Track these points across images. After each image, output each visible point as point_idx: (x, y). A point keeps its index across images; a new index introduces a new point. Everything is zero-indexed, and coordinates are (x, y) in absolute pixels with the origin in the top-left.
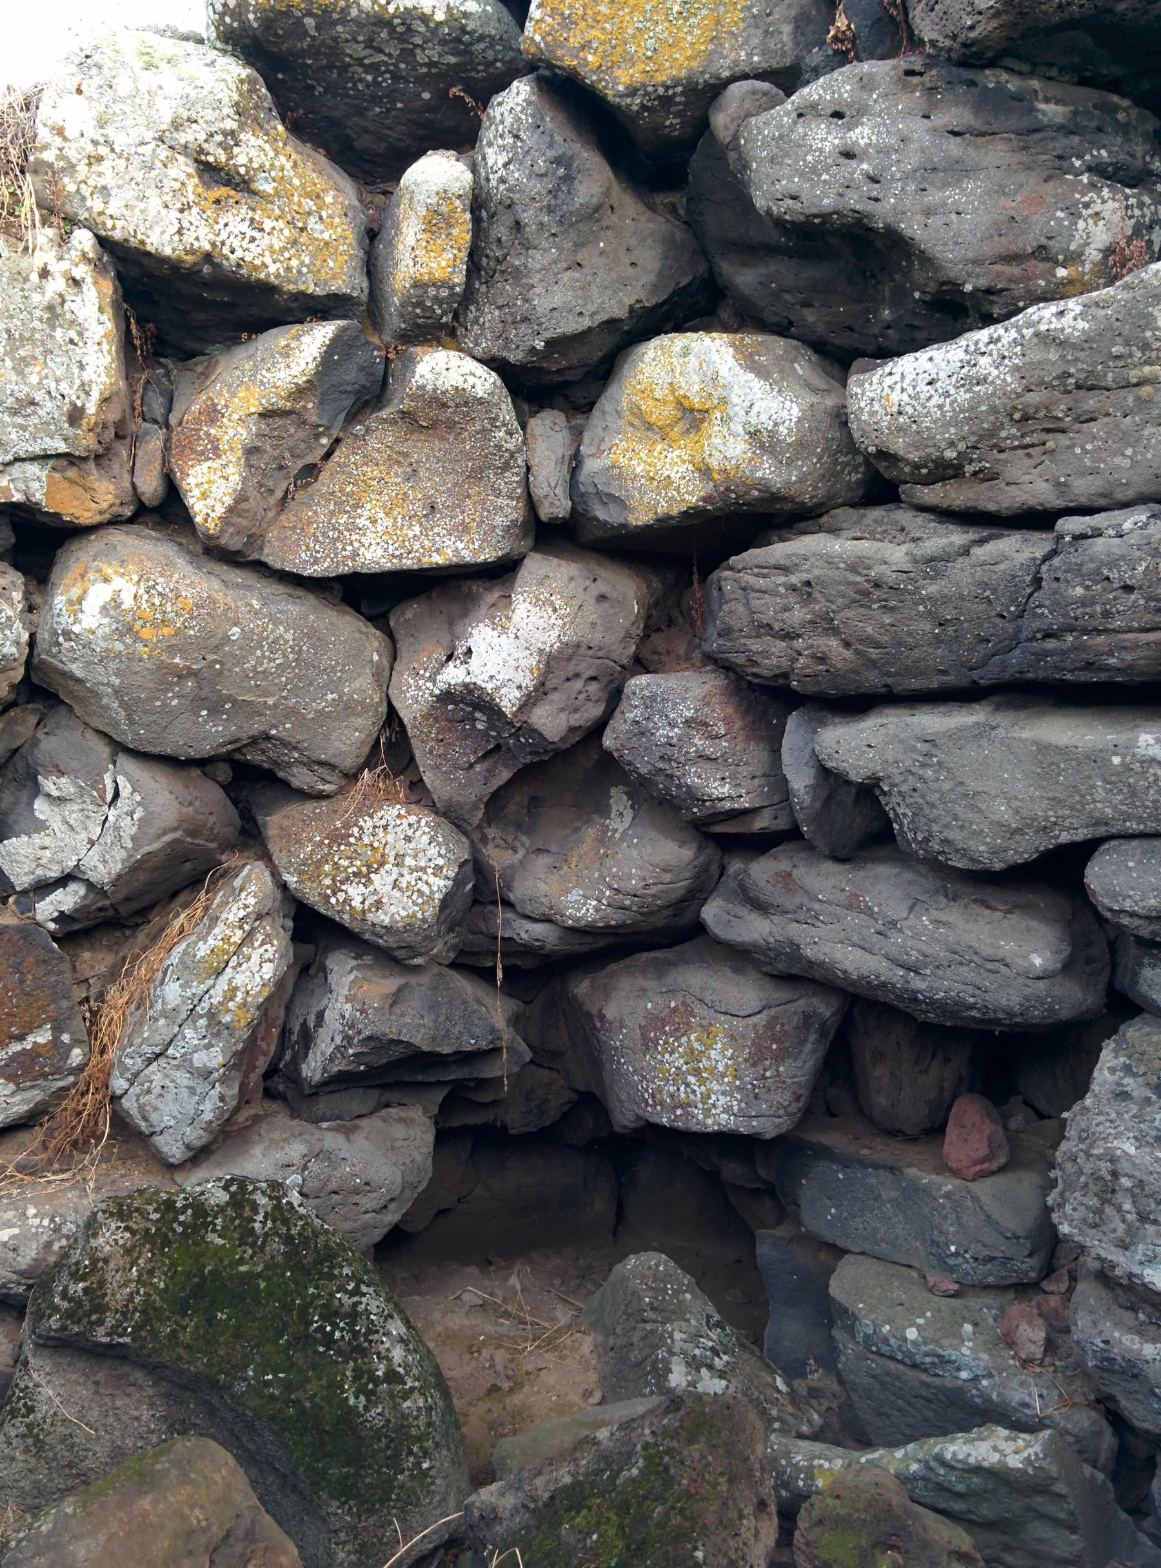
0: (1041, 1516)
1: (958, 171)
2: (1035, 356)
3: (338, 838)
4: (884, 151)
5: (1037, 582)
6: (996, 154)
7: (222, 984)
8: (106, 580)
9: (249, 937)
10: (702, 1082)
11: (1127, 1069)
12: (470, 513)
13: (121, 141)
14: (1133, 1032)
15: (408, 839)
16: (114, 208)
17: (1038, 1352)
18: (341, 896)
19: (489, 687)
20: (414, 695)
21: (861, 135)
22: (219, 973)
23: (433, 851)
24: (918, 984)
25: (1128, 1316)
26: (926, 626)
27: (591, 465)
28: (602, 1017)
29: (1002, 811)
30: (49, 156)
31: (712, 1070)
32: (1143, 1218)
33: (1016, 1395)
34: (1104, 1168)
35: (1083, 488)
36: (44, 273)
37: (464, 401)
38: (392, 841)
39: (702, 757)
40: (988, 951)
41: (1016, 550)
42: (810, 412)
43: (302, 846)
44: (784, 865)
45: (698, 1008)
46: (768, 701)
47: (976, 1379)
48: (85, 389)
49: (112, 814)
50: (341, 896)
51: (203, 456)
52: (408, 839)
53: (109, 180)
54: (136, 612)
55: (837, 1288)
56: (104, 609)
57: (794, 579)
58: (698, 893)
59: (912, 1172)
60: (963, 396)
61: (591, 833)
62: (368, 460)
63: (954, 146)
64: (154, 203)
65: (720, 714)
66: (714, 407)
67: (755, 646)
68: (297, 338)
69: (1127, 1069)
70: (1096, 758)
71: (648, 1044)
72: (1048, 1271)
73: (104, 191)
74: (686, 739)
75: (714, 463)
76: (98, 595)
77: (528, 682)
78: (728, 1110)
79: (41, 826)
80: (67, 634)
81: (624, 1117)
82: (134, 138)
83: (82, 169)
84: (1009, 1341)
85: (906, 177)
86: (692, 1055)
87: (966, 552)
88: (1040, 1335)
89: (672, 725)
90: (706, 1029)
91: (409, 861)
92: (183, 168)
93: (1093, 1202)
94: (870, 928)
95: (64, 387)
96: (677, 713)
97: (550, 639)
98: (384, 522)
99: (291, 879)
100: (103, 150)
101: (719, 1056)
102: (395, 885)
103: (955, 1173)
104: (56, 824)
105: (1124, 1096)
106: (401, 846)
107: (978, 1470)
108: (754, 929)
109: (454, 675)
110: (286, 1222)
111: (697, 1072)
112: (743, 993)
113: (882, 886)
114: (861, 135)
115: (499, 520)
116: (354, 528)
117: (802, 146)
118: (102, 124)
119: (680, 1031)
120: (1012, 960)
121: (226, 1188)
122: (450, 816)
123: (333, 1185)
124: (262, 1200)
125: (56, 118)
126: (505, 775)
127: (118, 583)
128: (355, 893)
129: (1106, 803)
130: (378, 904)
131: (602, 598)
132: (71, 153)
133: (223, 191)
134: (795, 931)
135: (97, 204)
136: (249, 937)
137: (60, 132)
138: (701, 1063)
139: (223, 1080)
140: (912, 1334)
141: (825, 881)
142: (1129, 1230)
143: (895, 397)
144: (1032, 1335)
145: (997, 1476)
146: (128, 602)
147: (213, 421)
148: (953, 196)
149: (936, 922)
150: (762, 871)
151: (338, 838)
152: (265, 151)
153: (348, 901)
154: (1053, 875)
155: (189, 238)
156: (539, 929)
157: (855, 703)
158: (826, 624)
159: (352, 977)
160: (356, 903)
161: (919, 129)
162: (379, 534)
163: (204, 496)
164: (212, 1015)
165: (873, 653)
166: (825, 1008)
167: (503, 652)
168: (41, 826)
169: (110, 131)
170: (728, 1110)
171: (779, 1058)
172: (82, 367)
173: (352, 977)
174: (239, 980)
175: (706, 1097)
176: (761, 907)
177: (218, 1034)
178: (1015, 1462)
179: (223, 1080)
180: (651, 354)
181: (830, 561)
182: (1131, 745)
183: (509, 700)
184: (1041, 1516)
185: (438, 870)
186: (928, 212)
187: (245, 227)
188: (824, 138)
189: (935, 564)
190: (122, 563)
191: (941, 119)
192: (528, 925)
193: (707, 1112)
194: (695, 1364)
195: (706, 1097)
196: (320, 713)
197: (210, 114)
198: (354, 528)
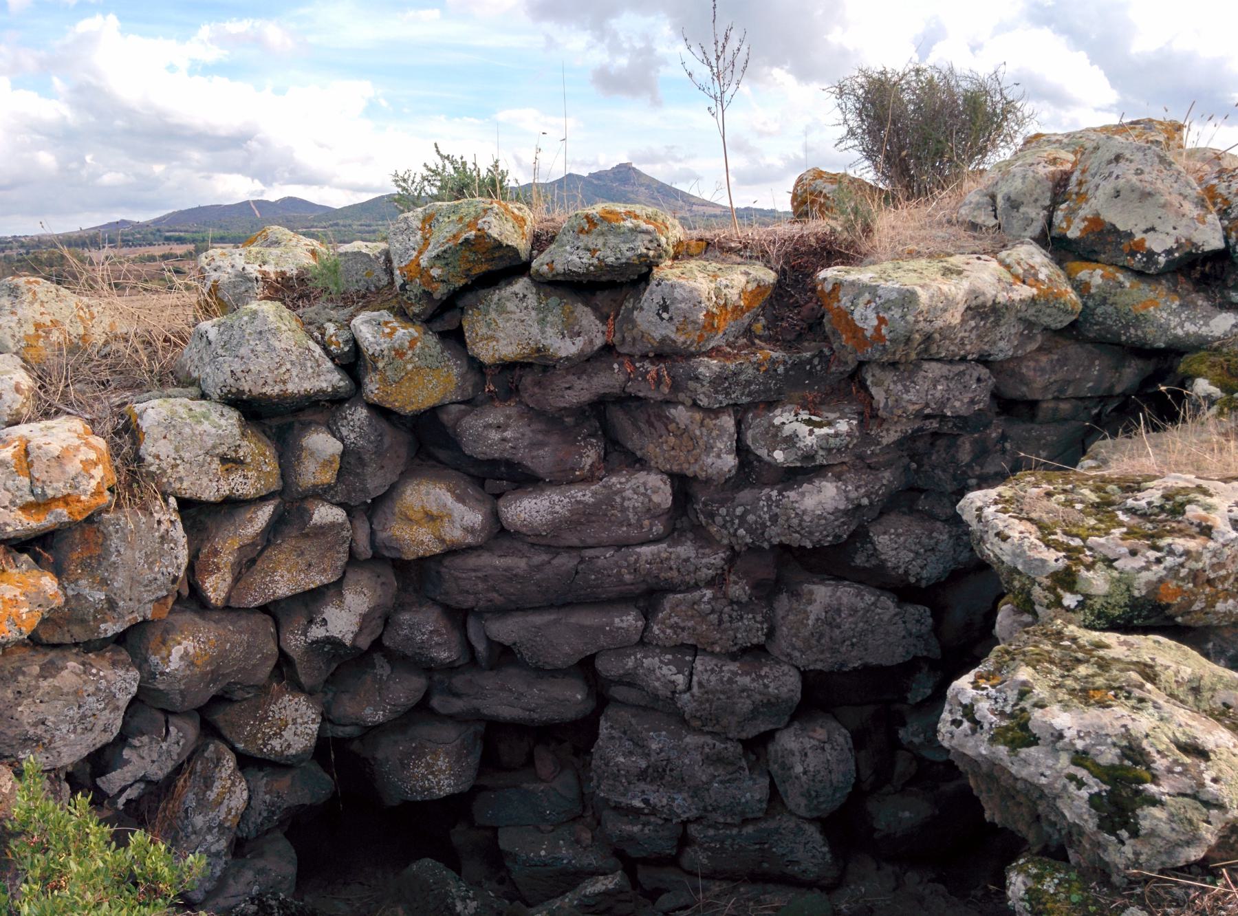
0: (620, 901)
1: (541, 445)
2: (575, 507)
3: (264, 719)
4: (516, 439)
5: (577, 573)
6: (554, 439)
7: (224, 809)
8: (180, 644)
9: (233, 784)
10: (435, 776)
11: (611, 727)
12: (327, 563)
13: (186, 456)
14: (610, 711)
15: (297, 710)
16: (185, 485)
17: (589, 842)
18: (269, 747)
19: (340, 636)
20: (295, 642)
21: (508, 434)
22: (221, 803)
23: (309, 712)
24: (536, 716)
25: (625, 819)
26: (534, 588)
27: (382, 535)
28: (374, 759)
29: (567, 649)
30: (153, 468)
31: (440, 771)
32: (629, 783)
33: (585, 862)
34: (615, 769)
35: (590, 541)
36: (159, 522)
37: (333, 525)
38: (289, 713)
39: (438, 644)
40: (561, 698)
41: (565, 562)
42: (484, 516)
43: (244, 728)
44: (468, 676)
45: (428, 744)
46: (458, 616)
47: (570, 861)
48: (179, 568)
49: (164, 745)
50: (269, 747)
51: (211, 573)
52: (297, 710)
53: (182, 473)
54: (195, 655)
55: (503, 844)
56: (181, 658)
57: (479, 574)
58: (427, 696)
59: (525, 785)
60: (549, 517)
61: (368, 678)
62: (280, 552)
63: (540, 437)
64: (205, 481)
65: (442, 625)
66: (436, 512)
67: (460, 598)
68: (255, 512)
69: (611, 727)
70: (601, 629)
71: (404, 766)
72: (585, 808)
73: (181, 479)
74: (430, 639)
75: (447, 538)
76: (177, 651)
77: (356, 629)
78: (449, 785)
79: (127, 762)
80: (162, 674)
81: (393, 800)
82: (194, 453)
83: (169, 471)
84: (578, 841)
85: (525, 447)
86: (428, 766)
87: (549, 562)
88: (590, 836)
89: (423, 634)
90: (434, 753)
91: (299, 721)
92: (216, 464)
93: (611, 782)
94: (509, 698)
95: (170, 569)
96: (424, 628)
97: (364, 608)
98: (287, 576)
99: (241, 746)
100: (178, 462)
101: (442, 763)
102: (295, 734)
103: (543, 781)
104: (135, 758)
105: (613, 738)
106: (295, 715)
107: (599, 894)
108: (458, 705)
109: (317, 632)
110: (288, 908)
111: (432, 773)
112: (450, 734)
113: (514, 679)
114: (508, 434)
115: (339, 563)
116: (272, 581)
117: (487, 438)
118: (177, 450)
119: (419, 758)
120: (572, 697)
121: (253, 903)
122: (310, 693)
123: (271, 883)
124: (273, 903)
125: (154, 450)
126: (335, 666)
127: (185, 643)
128: (276, 743)
129: (603, 641)
130: (289, 746)
131: (383, 584)
132: (164, 465)
133: (230, 465)
134: (477, 703)
135: (178, 485)
136: (233, 784)
137: (158, 457)
138: (437, 771)
139: (226, 855)
140: (543, 853)
141: (489, 681)
142: (626, 789)
143: (522, 515)
144: (586, 836)
145: (607, 893)
146: (191, 651)
147: (216, 556)
148: (541, 452)
149: (540, 690)
150: (458, 682)
151: (264, 719)
152: (249, 448)
153: (273, 748)
154: (586, 667)
155: (222, 492)
156: (348, 730)
157: (503, 611)
158: (494, 589)
159: (264, 781)
160: (278, 748)
161: (527, 431)
162: (283, 581)
163: (215, 590)
164: (221, 825)
165: (513, 598)
166: (480, 728)
167: (342, 621)
168: (127, 762)
169: (182, 453)
170: (449, 785)
171: (467, 756)
172: (176, 558)
173: (264, 781)
174: (232, 804)
175: (438, 783)
176: (457, 695)
177: (223, 834)
178: (611, 886)
179: (226, 855)
180: (409, 492)
181: (496, 568)
182: (613, 623)
183: (348, 642)
184: (620, 901)
185: (313, 721)
186: (533, 458)
187: (241, 480)
188: (494, 435)
189: (538, 568)
190: (182, 632)
191: (534, 427)
192: (341, 728)
193: (440, 790)
194: (464, 899)
195: (438, 783)
196: (254, 666)
197: (230, 440)
198: (272, 581)
